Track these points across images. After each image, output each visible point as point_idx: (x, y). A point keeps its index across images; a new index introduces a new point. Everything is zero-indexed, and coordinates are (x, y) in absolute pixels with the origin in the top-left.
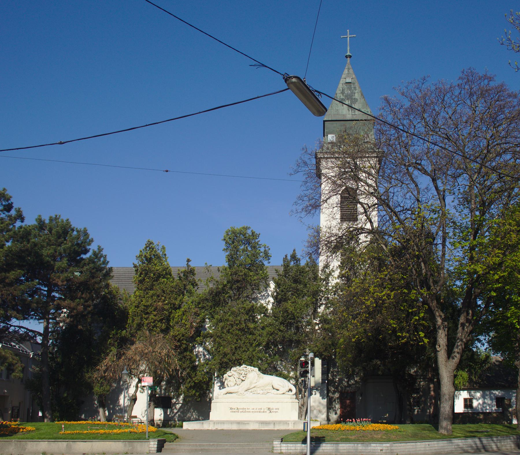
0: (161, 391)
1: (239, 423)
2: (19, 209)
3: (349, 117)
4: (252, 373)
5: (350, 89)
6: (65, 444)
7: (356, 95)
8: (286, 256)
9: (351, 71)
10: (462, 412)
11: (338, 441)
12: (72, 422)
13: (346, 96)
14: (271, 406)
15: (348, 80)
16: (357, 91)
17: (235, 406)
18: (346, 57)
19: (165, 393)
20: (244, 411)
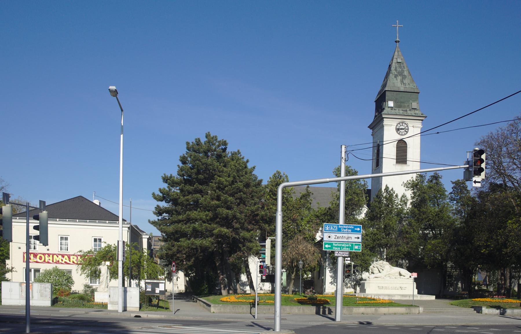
0: (269, 272)
1: (389, 295)
2: (199, 139)
3: (402, 89)
4: (386, 265)
5: (400, 67)
6: (374, 309)
7: (405, 72)
8: (178, 166)
9: (400, 53)
10: (6, 274)
11: (513, 308)
12: (476, 299)
13: (398, 73)
14: (402, 286)
15: (399, 60)
16: (405, 70)
17: (380, 285)
18: (396, 42)
19: (272, 273)
20: (386, 288)
